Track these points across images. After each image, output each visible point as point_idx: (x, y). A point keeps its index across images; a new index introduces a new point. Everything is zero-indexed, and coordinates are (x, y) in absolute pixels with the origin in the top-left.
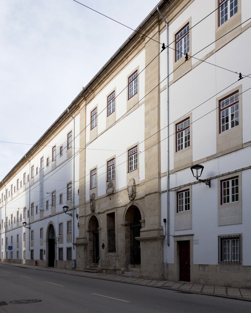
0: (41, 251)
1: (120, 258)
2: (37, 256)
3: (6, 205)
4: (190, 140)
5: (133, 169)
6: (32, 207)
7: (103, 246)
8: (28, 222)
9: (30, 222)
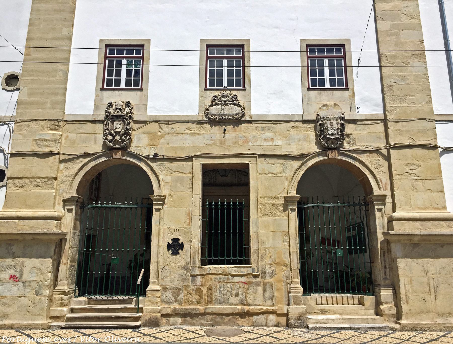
1: (268, 280)
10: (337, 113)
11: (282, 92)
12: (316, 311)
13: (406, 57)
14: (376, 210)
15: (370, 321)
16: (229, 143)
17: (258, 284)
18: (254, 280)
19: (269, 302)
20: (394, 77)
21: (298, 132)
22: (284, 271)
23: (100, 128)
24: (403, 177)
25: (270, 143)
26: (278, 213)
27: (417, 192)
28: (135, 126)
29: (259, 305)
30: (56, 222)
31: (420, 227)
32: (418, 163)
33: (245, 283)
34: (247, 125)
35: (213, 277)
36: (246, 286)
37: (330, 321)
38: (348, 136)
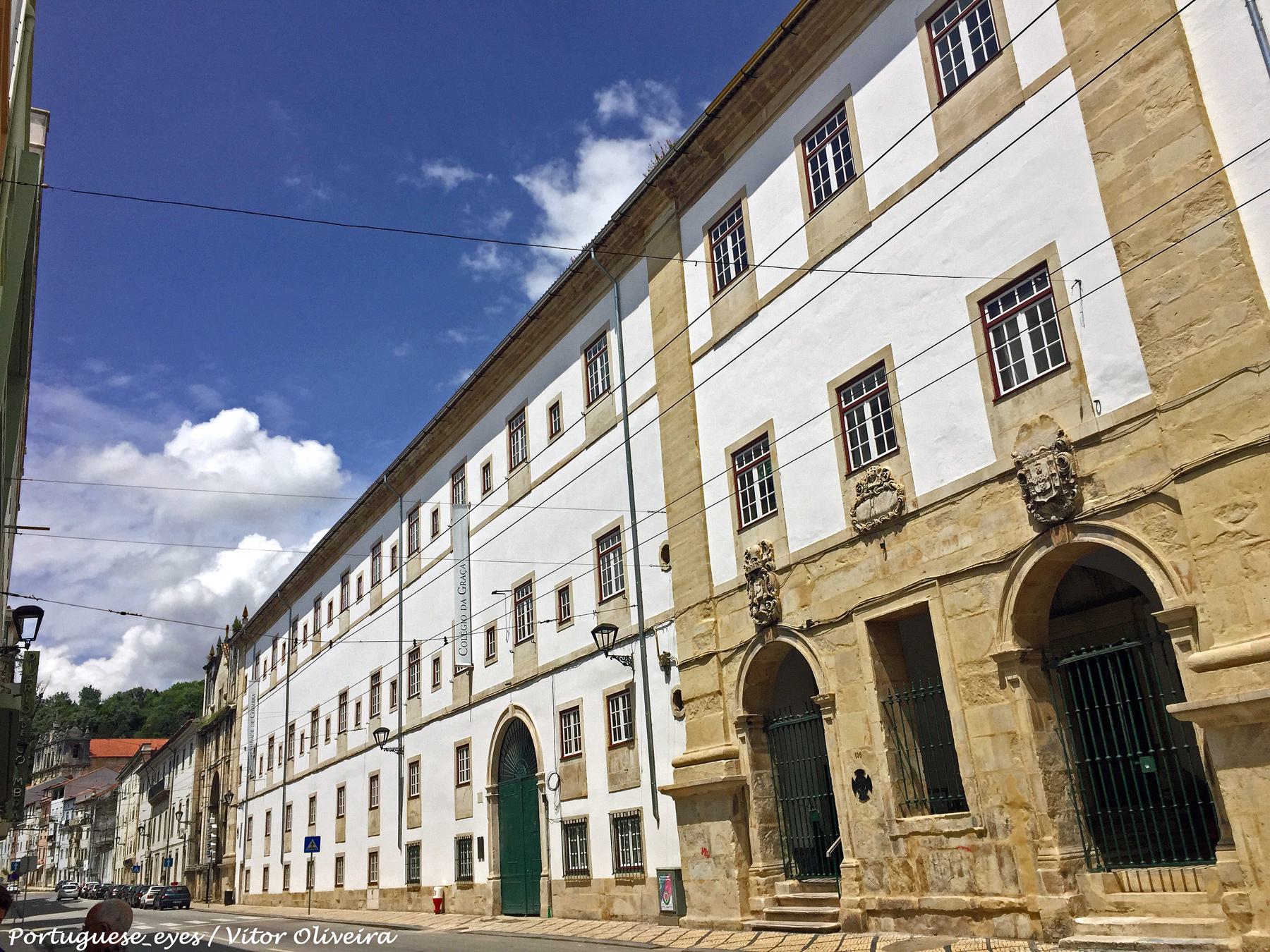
0: (463, 844)
1: (1003, 840)
2: (439, 872)
3: (406, 593)
4: (776, 491)
5: (760, 515)
6: (411, 666)
7: (862, 785)
8: (394, 729)
9: (400, 728)
10: (1047, 437)
11: (955, 427)
12: (1108, 908)
13: (1173, 220)
14: (1176, 648)
15: (1198, 931)
16: (895, 569)
17: (988, 852)
18: (980, 843)
19: (1012, 889)
20: (1154, 290)
21: (995, 506)
22: (1025, 820)
23: (743, 598)
24: (1217, 548)
25: (953, 548)
26: (994, 695)
27: (1257, 579)
28: (781, 578)
29: (997, 895)
30: (724, 762)
31: (1258, 679)
32: (1248, 497)
33: (968, 849)
34: (913, 522)
35: (919, 838)
36: (970, 854)
37: (1115, 928)
38: (1089, 479)
